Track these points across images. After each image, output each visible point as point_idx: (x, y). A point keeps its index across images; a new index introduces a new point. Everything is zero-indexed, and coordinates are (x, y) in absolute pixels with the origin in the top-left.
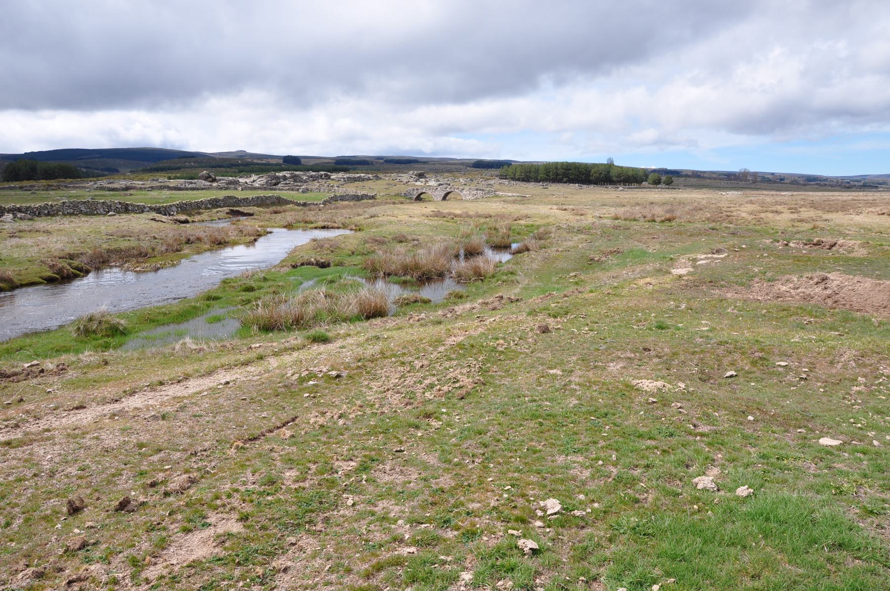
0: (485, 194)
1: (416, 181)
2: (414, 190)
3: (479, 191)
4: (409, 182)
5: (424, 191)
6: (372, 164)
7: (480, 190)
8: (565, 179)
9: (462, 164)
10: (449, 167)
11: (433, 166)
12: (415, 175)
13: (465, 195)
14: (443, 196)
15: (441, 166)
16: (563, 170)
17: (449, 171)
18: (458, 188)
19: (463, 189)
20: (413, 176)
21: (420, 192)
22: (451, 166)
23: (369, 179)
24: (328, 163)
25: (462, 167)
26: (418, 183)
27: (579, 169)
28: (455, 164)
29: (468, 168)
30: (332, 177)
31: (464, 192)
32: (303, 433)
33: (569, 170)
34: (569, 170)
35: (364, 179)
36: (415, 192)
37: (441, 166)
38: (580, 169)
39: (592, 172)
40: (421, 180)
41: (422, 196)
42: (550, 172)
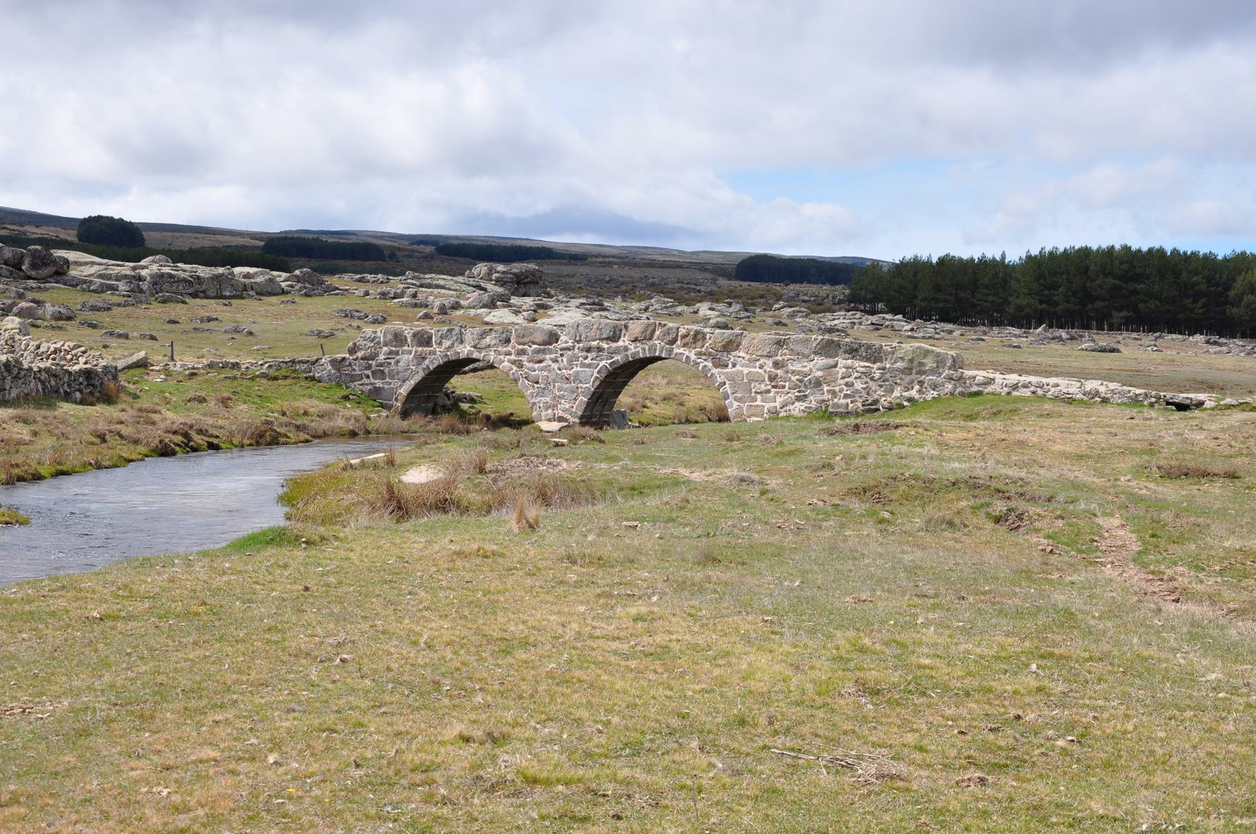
0: (887, 382)
1: (491, 305)
2: (399, 339)
3: (843, 362)
4: (456, 306)
5: (464, 350)
6: (392, 256)
7: (853, 351)
8: (1118, 316)
9: (702, 267)
10: (656, 275)
11: (602, 271)
12: (499, 282)
13: (745, 386)
14: (589, 385)
15: (628, 273)
16: (1111, 280)
17: (659, 288)
18: (698, 337)
19: (730, 346)
20: (489, 286)
21: (438, 354)
22: (665, 273)
23: (269, 290)
24: (244, 247)
25: (700, 276)
26: (500, 315)
27: (1177, 274)
28: (678, 266)
29: (722, 282)
30: (74, 272)
31: (741, 364)
32: (407, 621)
33: (1138, 278)
34: (1138, 278)
35: (245, 288)
36: (406, 358)
37: (628, 273)
38: (1184, 276)
39: (1239, 284)
40: (514, 300)
41: (459, 384)
42: (1054, 287)
